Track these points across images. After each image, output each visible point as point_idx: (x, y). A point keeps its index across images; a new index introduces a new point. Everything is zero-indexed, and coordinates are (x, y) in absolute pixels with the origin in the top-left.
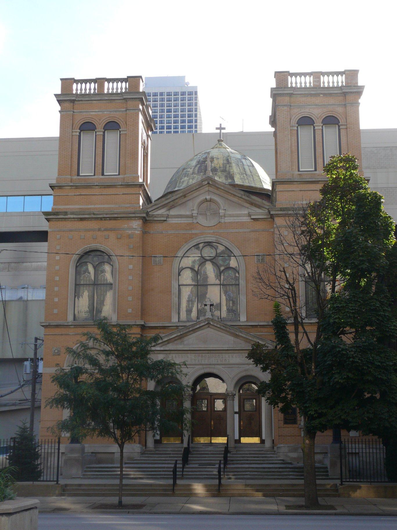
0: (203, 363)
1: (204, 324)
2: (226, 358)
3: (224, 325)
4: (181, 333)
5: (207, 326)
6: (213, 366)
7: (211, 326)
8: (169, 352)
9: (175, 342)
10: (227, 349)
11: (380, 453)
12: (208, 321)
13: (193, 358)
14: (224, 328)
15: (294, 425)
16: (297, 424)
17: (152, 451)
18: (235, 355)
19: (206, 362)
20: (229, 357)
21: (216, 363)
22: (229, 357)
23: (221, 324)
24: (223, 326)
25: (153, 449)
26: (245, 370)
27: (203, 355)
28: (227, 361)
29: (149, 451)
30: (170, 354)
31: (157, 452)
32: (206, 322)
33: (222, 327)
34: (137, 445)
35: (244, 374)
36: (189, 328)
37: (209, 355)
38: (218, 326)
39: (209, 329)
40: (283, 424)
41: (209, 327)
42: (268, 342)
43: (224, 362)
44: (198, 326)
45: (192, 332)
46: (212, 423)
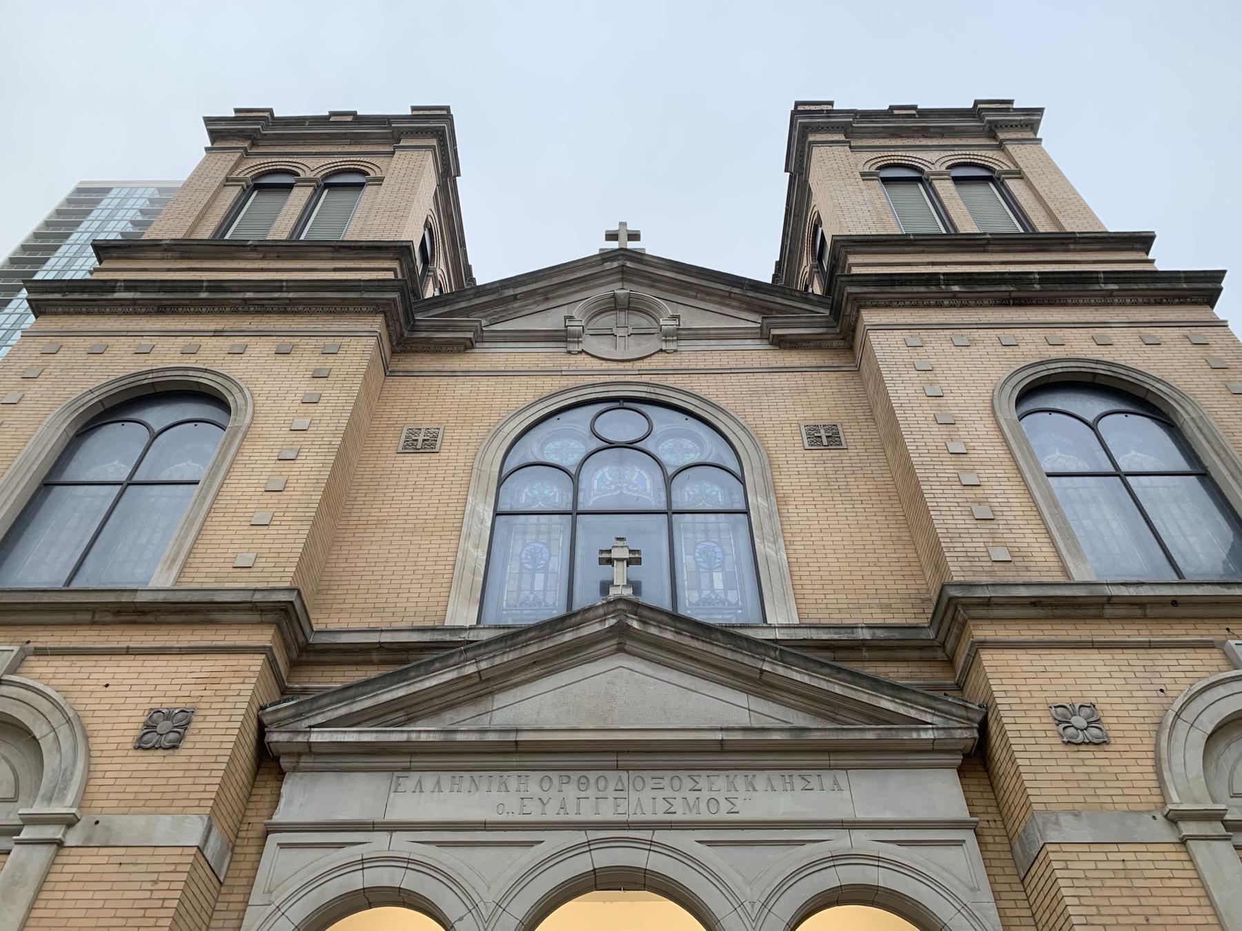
0: (588, 815)
2: (713, 795)
8: (404, 761)
19: (608, 815)
26: (836, 859)
28: (725, 806)
32: (611, 622)
41: (621, 649)
43: (705, 816)
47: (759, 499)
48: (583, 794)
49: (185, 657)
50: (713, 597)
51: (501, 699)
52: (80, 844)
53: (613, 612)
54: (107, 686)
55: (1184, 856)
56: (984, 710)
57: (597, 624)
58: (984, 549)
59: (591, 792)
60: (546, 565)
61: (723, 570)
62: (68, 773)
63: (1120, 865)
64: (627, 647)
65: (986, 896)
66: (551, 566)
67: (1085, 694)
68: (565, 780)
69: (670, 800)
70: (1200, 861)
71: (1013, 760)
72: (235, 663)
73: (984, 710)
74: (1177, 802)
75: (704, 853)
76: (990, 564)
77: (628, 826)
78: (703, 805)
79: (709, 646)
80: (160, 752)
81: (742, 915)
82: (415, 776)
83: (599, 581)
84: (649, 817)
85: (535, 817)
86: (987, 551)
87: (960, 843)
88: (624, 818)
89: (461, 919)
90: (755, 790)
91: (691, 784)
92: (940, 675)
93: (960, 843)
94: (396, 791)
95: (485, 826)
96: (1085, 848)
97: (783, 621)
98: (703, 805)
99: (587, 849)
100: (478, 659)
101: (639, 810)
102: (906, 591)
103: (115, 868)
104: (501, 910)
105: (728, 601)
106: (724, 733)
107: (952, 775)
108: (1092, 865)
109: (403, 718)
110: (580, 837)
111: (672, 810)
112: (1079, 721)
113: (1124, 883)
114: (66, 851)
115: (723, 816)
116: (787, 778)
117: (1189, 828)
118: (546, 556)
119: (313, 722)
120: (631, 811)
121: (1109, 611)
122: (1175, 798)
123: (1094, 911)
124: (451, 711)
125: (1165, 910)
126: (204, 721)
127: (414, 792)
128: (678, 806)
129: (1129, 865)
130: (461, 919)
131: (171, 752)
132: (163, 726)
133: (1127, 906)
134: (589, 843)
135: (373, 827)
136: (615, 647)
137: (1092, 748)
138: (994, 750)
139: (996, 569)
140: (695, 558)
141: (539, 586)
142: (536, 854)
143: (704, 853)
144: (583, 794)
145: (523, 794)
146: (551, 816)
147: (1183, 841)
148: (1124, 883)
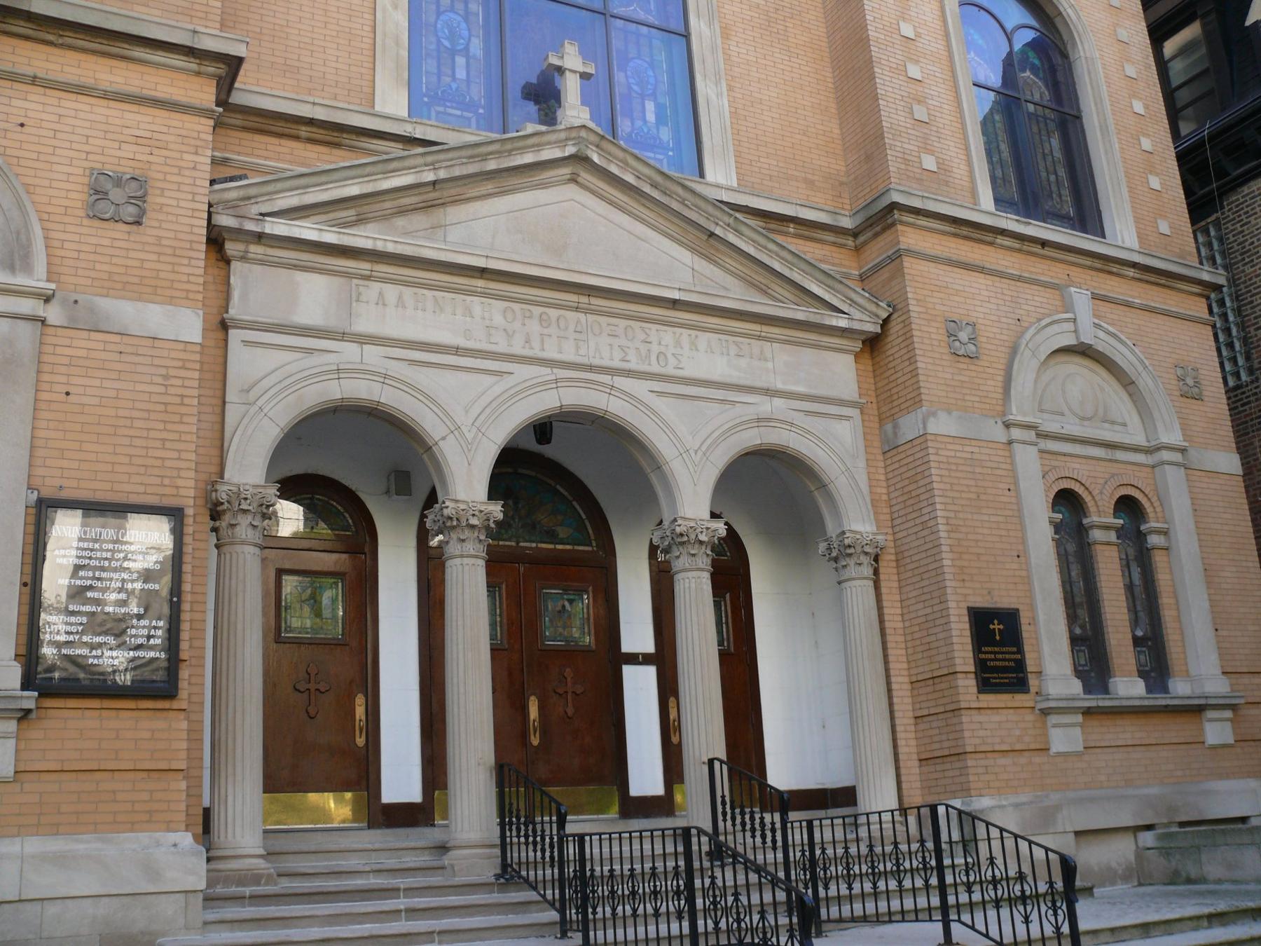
0: (551, 353)
1: (557, 153)
2: (663, 349)
3: (658, 179)
4: (442, 174)
5: (565, 171)
6: (606, 379)
7: (585, 176)
8: (364, 266)
9: (400, 222)
10: (676, 295)
11: (726, 834)
12: (579, 141)
13: (498, 319)
14: (655, 194)
15: (1019, 699)
16: (1027, 691)
17: (256, 879)
18: (704, 337)
19: (569, 355)
20: (678, 344)
21: (616, 363)
22: (678, 344)
23: (646, 171)
24: (655, 185)
25: (261, 863)
26: (761, 421)
27: (553, 313)
28: (672, 361)
29: (241, 882)
30: (368, 278)
31: (285, 885)
32: (570, 150)
33: (647, 189)
34: (173, 837)
35: (752, 438)
36: (484, 158)
37: (582, 316)
38: (630, 178)
39: (572, 191)
40: (975, 690)
41: (574, 180)
42: (854, 296)
43: (655, 368)
44: (528, 158)
45: (489, 187)
46: (534, 712)
47: (702, 24)
48: (546, 331)
49: (112, 104)
50: (646, 130)
51: (455, 213)
52: (66, 325)
53: (574, 139)
54: (22, 125)
55: (1007, 454)
56: (891, 310)
57: (557, 150)
58: (917, 154)
59: (553, 330)
60: (467, 48)
61: (655, 100)
62: (23, 237)
63: (969, 456)
64: (579, 179)
65: (862, 464)
66: (472, 50)
67: (970, 313)
68: (528, 314)
69: (625, 349)
70: (1018, 459)
71: (912, 360)
72: (178, 124)
73: (891, 310)
74: (1016, 415)
75: (659, 404)
76: (919, 171)
77: (591, 368)
78: (654, 358)
79: (668, 198)
80: (121, 226)
81: (687, 460)
82: (376, 287)
83: (523, 83)
84: (606, 362)
85: (502, 347)
86: (919, 157)
87: (848, 418)
88: (585, 361)
89: (443, 438)
90: (697, 350)
91: (643, 336)
92: (846, 263)
93: (848, 418)
94: (358, 301)
95: (457, 351)
96: (951, 440)
97: (721, 180)
98: (654, 358)
99: (554, 386)
100: (437, 166)
101: (597, 355)
102: (828, 170)
103: (116, 357)
104: (453, 429)
105: (660, 139)
106: (682, 293)
107: (851, 358)
108: (953, 454)
109: (354, 218)
110: (545, 373)
111: (627, 358)
112: (964, 336)
113: (969, 469)
114: (50, 331)
115: (670, 370)
116: (724, 343)
117: (1016, 433)
118: (465, 33)
119: (266, 208)
120: (591, 354)
121: (1000, 240)
122: (1014, 410)
123: (948, 487)
124: (402, 218)
125: (989, 491)
126: (162, 195)
127: (377, 304)
128: (632, 356)
129: (975, 456)
130: (443, 438)
131: (134, 228)
132: (116, 195)
133: (968, 486)
134: (556, 381)
135: (343, 336)
136: (568, 176)
137: (967, 360)
138: (889, 346)
139: (925, 178)
140: (627, 77)
141: (461, 74)
142: (508, 382)
143: (659, 404)
144: (546, 331)
145: (488, 323)
146: (518, 349)
147: (1010, 443)
148: (969, 469)
